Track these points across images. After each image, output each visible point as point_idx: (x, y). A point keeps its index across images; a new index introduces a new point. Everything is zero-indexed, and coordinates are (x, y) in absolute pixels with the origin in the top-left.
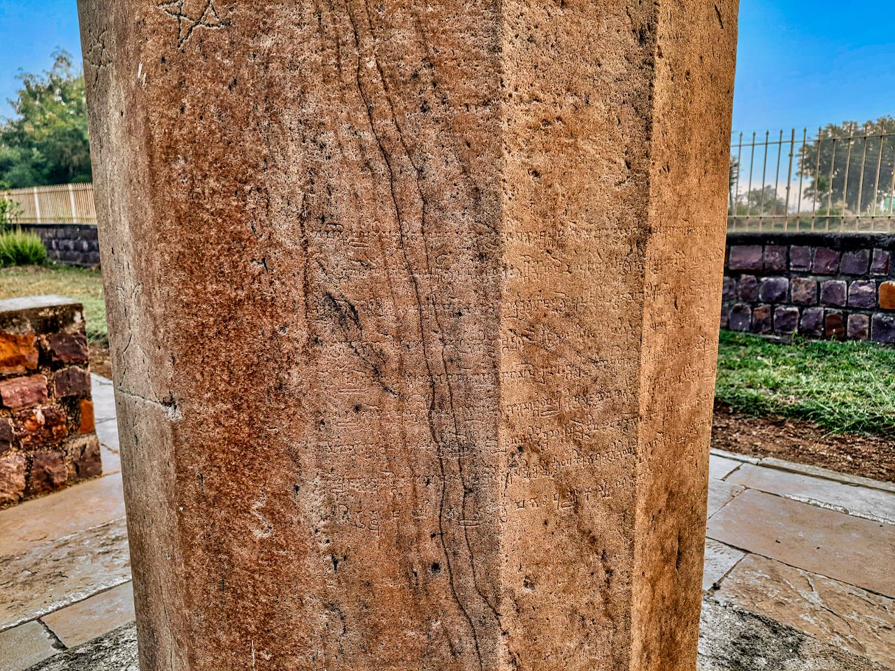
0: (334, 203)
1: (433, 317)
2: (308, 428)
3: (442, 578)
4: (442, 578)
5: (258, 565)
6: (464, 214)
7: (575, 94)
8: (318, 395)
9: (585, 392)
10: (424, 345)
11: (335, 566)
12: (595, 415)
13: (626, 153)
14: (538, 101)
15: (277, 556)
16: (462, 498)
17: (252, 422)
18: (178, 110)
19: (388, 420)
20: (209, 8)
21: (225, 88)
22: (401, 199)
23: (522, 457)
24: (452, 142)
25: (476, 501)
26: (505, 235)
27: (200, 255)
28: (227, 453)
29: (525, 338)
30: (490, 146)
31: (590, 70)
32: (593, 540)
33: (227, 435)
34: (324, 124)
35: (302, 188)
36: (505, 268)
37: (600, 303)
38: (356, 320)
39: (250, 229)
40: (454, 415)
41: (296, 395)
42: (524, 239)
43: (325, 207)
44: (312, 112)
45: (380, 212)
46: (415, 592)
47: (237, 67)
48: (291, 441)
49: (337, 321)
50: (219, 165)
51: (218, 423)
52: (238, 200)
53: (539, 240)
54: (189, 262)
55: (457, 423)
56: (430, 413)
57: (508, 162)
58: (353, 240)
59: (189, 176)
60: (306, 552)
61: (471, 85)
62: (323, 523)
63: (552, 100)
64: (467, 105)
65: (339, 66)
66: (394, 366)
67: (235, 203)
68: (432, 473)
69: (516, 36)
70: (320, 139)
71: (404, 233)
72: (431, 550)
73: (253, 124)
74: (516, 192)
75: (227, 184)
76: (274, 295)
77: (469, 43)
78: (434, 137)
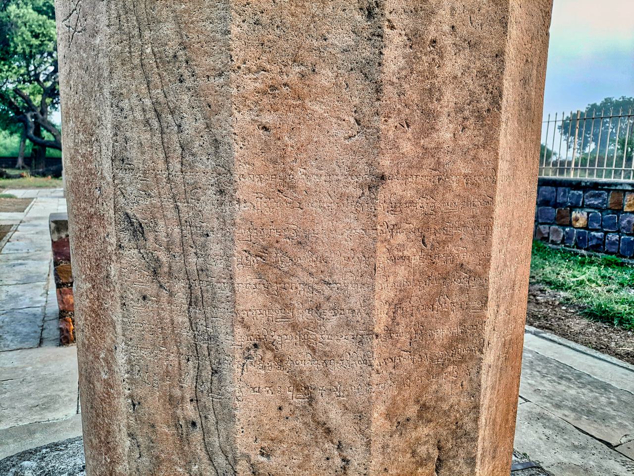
0: (129, 149)
3: (197, 435)
4: (197, 435)
6: (208, 159)
9: (318, 307)
11: (134, 408)
12: (329, 327)
13: (355, 112)
14: (265, 71)
16: (210, 377)
26: (237, 176)
29: (259, 259)
31: (316, 44)
32: (328, 431)
34: (122, 94)
38: (143, 233)
40: (205, 312)
45: (155, 156)
46: (181, 440)
55: (206, 319)
56: (189, 308)
61: (210, 61)
63: (279, 70)
64: (208, 77)
66: (166, 269)
68: (191, 354)
70: (120, 104)
72: (190, 411)
77: (208, 29)
78: (187, 100)
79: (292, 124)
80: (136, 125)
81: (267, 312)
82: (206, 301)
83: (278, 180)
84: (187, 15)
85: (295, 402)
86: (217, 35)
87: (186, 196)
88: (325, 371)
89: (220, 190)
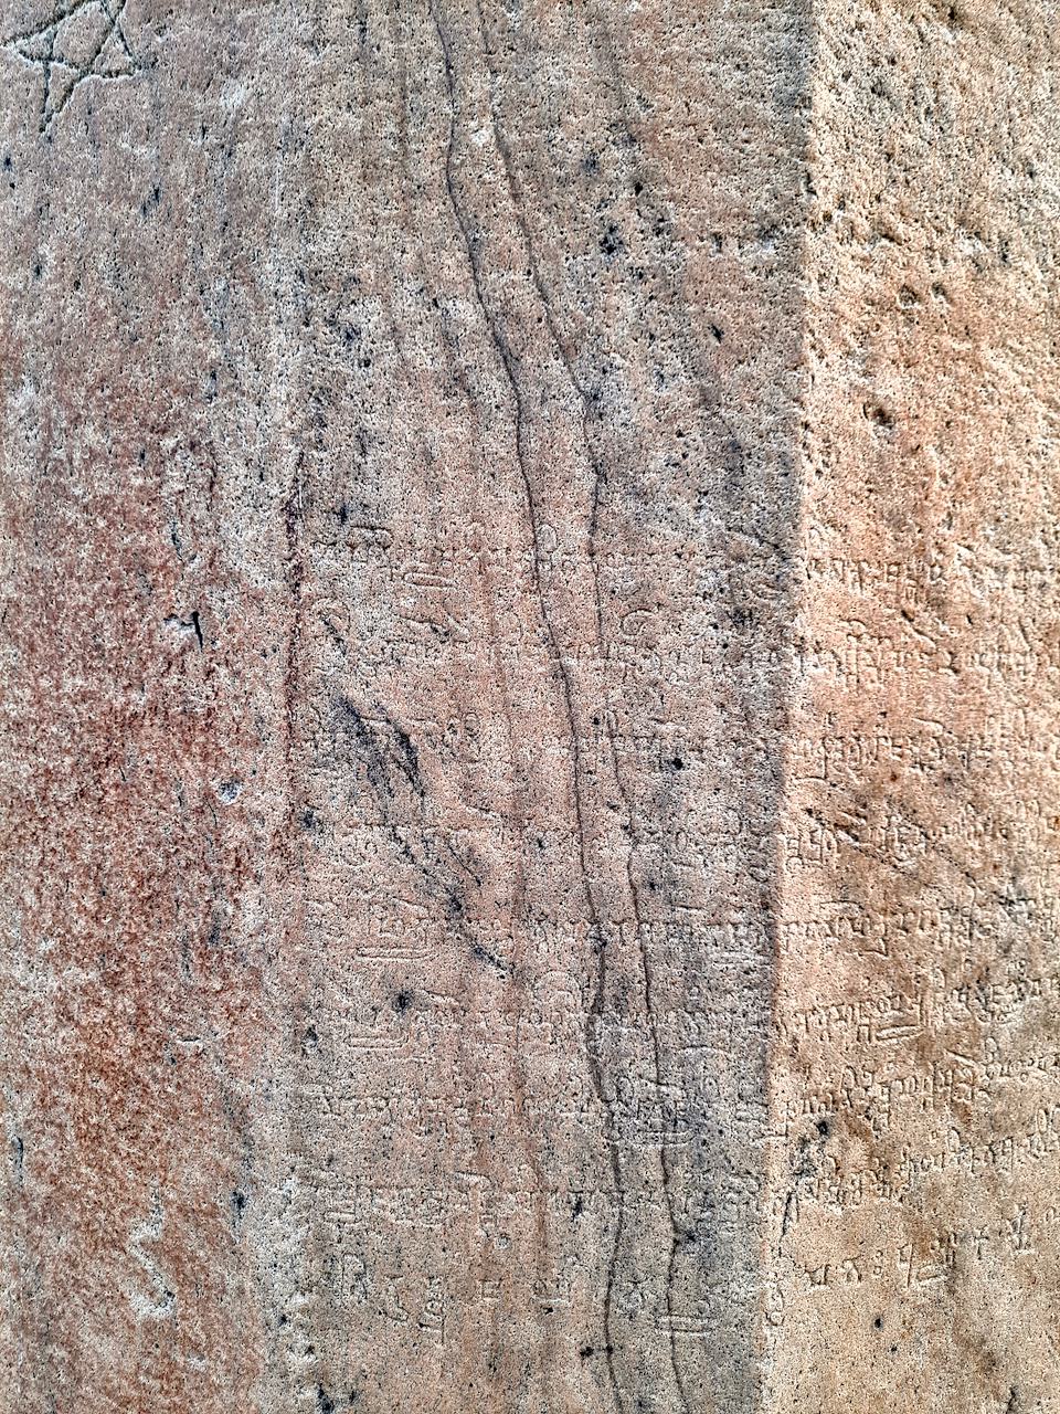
1: (610, 770)
2: (275, 1047)
5: (138, 1386)
7: (977, 234)
8: (303, 962)
9: (983, 978)
10: (581, 841)
12: (1005, 1038)
14: (892, 240)
15: (184, 1370)
16: (666, 1257)
17: (144, 1020)
18: (30, 273)
19: (479, 1034)
20: (114, 35)
21: (134, 211)
22: (541, 468)
23: (827, 1150)
24: (675, 327)
25: (705, 1266)
26: (803, 565)
27: (53, 606)
28: (81, 1094)
29: (842, 835)
30: (772, 339)
32: (990, 1363)
33: (83, 1047)
34: (356, 280)
35: (293, 435)
36: (801, 649)
37: (1023, 753)
38: (412, 769)
39: (168, 541)
40: (653, 1031)
41: (249, 959)
42: (850, 577)
43: (351, 484)
44: (331, 250)
45: (485, 501)
47: (164, 161)
48: (233, 1076)
49: (363, 772)
50: (108, 392)
51: (65, 1016)
52: (145, 475)
53: (884, 585)
54: (27, 624)
56: (591, 1022)
57: (817, 381)
58: (415, 570)
59: (43, 420)
60: (253, 1372)
61: (729, 188)
62: (299, 1300)
63: (925, 242)
64: (718, 238)
65: (401, 140)
66: (502, 891)
67: (138, 482)
68: (589, 1185)
69: (846, 77)
70: (347, 316)
71: (543, 553)
73: (190, 292)
74: (833, 458)
75: (124, 437)
76: (214, 704)
77: (729, 86)
79: (947, 408)
80: (410, 391)
81: (857, 1011)
82: (663, 994)
83: (904, 580)
84: (649, 33)
85: (915, 1293)
86: (761, 106)
87: (600, 636)
88: (991, 1178)
89: (737, 611)
